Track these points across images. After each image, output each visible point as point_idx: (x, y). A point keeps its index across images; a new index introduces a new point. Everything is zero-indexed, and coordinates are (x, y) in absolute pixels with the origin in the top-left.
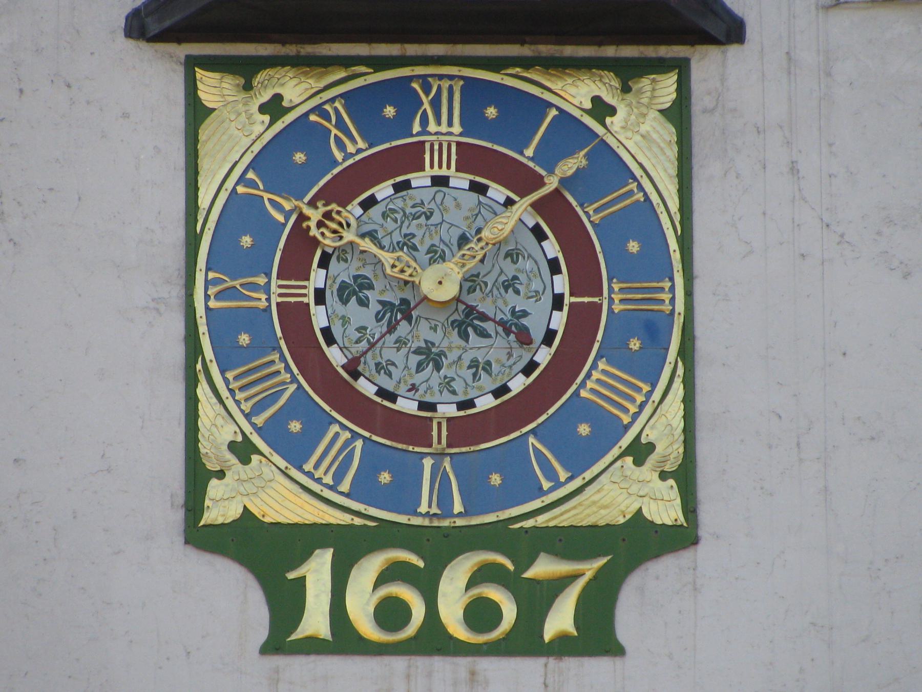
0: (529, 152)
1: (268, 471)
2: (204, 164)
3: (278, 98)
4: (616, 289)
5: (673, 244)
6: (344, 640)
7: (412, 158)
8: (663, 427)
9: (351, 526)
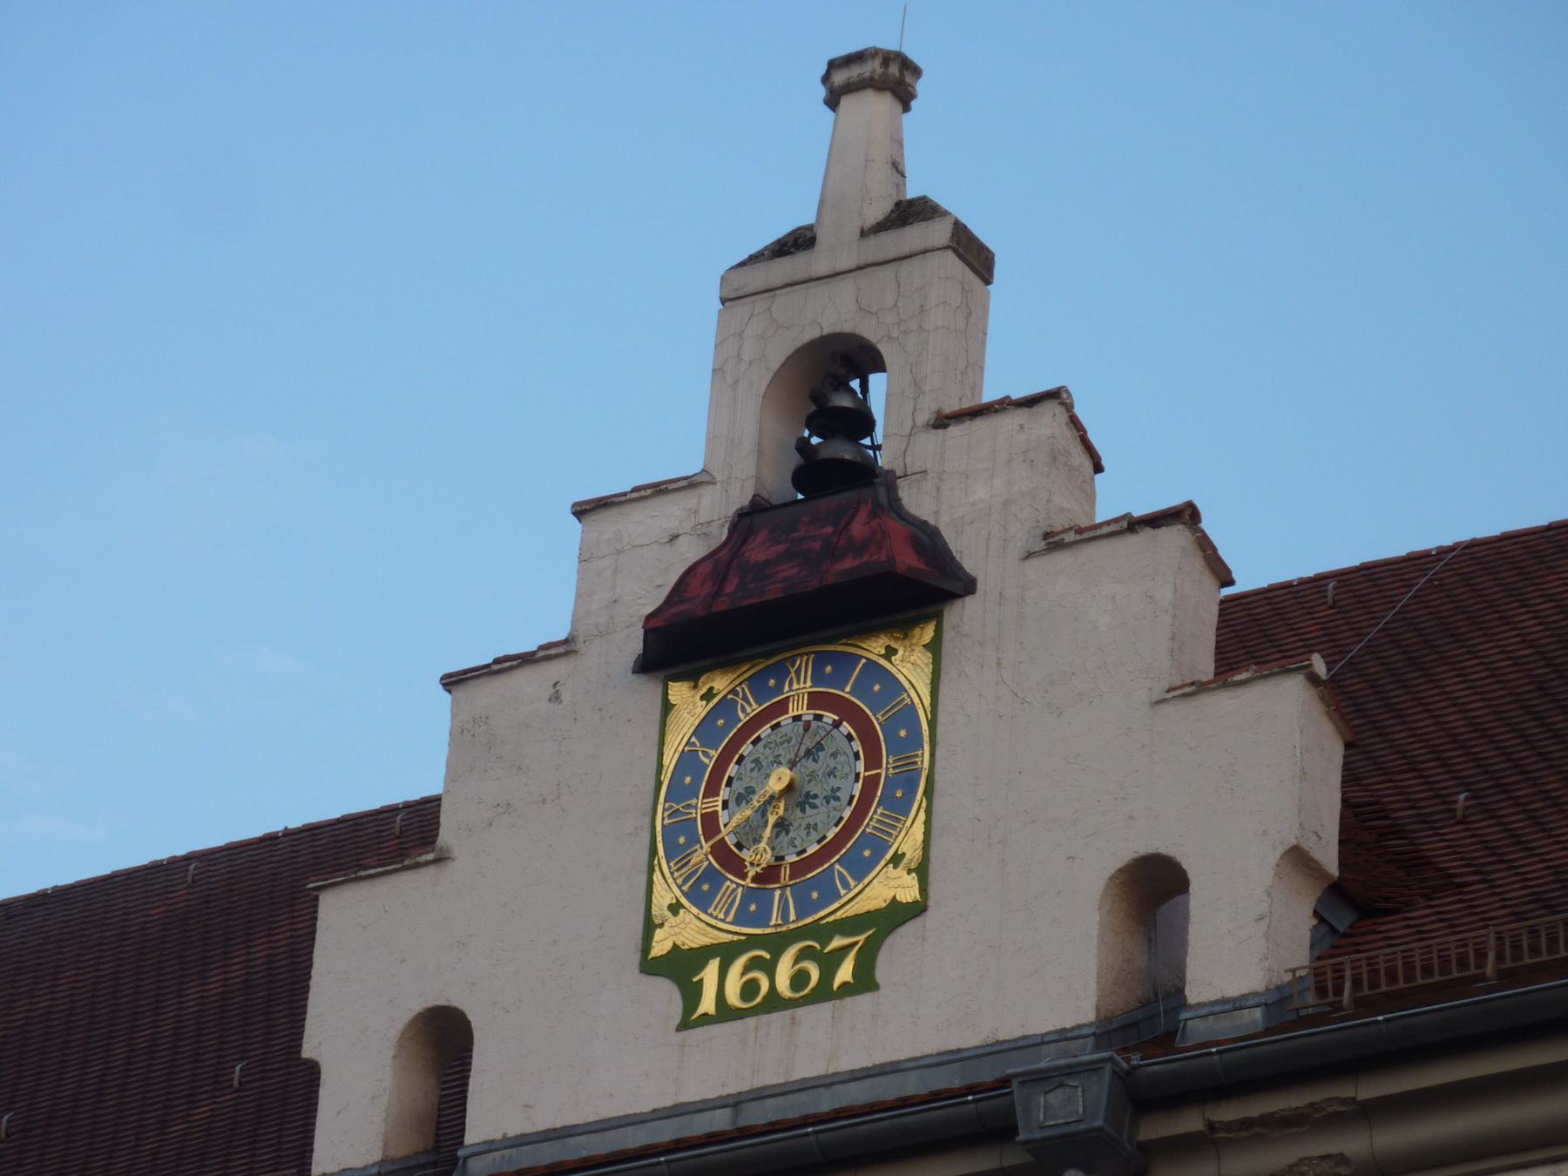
0: (848, 689)
1: (689, 918)
2: (668, 738)
3: (711, 688)
4: (895, 766)
5: (925, 726)
6: (725, 1013)
7: (782, 707)
8: (910, 840)
9: (732, 942)
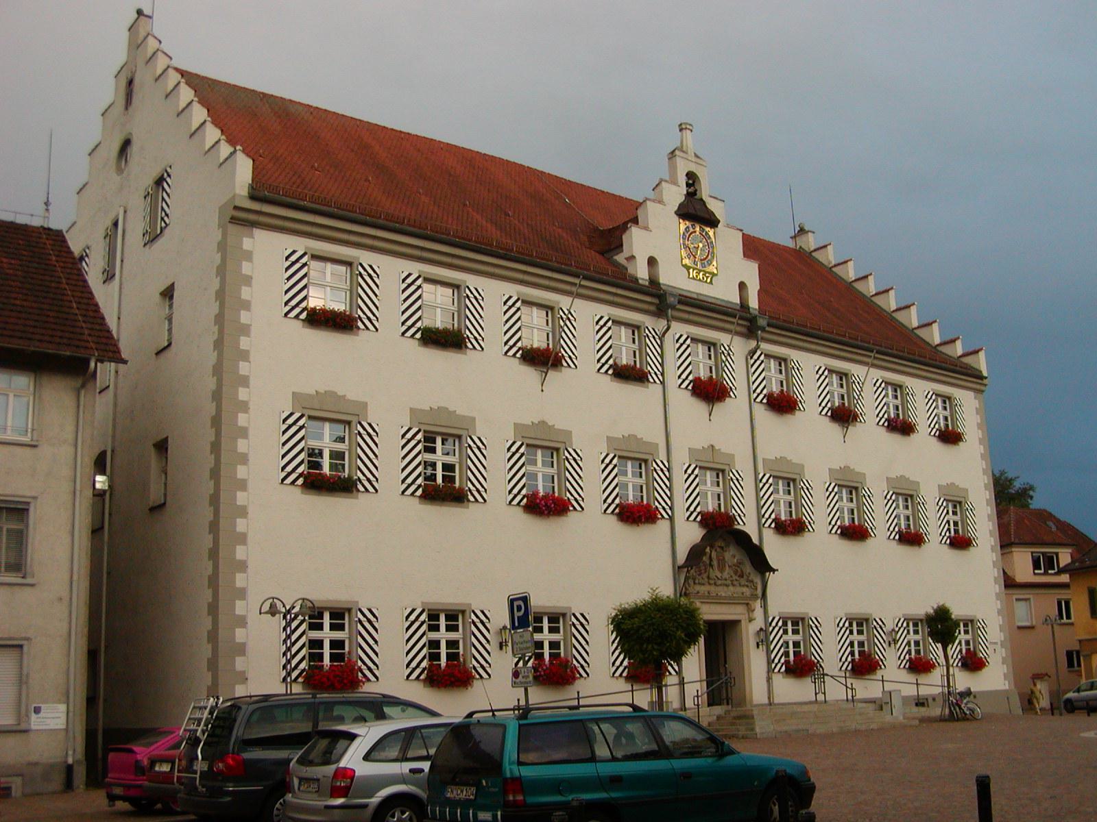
6: (693, 278)
